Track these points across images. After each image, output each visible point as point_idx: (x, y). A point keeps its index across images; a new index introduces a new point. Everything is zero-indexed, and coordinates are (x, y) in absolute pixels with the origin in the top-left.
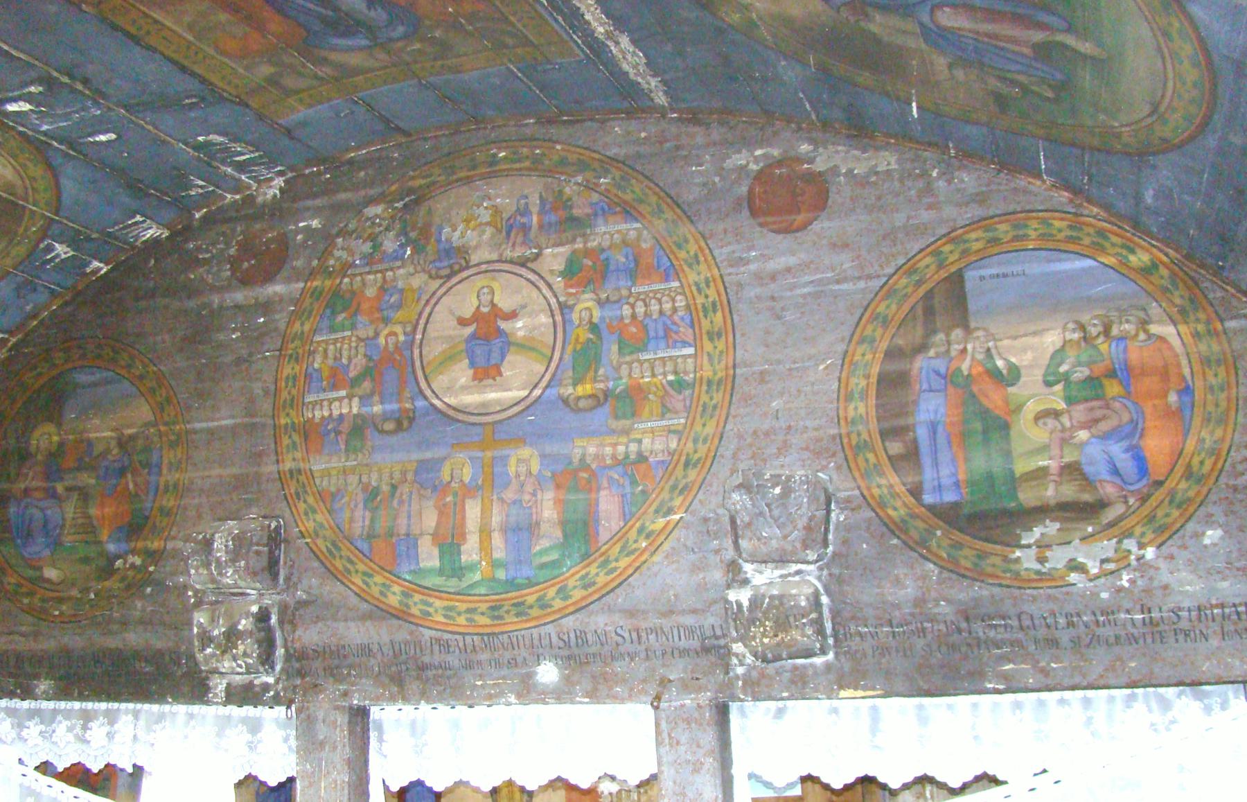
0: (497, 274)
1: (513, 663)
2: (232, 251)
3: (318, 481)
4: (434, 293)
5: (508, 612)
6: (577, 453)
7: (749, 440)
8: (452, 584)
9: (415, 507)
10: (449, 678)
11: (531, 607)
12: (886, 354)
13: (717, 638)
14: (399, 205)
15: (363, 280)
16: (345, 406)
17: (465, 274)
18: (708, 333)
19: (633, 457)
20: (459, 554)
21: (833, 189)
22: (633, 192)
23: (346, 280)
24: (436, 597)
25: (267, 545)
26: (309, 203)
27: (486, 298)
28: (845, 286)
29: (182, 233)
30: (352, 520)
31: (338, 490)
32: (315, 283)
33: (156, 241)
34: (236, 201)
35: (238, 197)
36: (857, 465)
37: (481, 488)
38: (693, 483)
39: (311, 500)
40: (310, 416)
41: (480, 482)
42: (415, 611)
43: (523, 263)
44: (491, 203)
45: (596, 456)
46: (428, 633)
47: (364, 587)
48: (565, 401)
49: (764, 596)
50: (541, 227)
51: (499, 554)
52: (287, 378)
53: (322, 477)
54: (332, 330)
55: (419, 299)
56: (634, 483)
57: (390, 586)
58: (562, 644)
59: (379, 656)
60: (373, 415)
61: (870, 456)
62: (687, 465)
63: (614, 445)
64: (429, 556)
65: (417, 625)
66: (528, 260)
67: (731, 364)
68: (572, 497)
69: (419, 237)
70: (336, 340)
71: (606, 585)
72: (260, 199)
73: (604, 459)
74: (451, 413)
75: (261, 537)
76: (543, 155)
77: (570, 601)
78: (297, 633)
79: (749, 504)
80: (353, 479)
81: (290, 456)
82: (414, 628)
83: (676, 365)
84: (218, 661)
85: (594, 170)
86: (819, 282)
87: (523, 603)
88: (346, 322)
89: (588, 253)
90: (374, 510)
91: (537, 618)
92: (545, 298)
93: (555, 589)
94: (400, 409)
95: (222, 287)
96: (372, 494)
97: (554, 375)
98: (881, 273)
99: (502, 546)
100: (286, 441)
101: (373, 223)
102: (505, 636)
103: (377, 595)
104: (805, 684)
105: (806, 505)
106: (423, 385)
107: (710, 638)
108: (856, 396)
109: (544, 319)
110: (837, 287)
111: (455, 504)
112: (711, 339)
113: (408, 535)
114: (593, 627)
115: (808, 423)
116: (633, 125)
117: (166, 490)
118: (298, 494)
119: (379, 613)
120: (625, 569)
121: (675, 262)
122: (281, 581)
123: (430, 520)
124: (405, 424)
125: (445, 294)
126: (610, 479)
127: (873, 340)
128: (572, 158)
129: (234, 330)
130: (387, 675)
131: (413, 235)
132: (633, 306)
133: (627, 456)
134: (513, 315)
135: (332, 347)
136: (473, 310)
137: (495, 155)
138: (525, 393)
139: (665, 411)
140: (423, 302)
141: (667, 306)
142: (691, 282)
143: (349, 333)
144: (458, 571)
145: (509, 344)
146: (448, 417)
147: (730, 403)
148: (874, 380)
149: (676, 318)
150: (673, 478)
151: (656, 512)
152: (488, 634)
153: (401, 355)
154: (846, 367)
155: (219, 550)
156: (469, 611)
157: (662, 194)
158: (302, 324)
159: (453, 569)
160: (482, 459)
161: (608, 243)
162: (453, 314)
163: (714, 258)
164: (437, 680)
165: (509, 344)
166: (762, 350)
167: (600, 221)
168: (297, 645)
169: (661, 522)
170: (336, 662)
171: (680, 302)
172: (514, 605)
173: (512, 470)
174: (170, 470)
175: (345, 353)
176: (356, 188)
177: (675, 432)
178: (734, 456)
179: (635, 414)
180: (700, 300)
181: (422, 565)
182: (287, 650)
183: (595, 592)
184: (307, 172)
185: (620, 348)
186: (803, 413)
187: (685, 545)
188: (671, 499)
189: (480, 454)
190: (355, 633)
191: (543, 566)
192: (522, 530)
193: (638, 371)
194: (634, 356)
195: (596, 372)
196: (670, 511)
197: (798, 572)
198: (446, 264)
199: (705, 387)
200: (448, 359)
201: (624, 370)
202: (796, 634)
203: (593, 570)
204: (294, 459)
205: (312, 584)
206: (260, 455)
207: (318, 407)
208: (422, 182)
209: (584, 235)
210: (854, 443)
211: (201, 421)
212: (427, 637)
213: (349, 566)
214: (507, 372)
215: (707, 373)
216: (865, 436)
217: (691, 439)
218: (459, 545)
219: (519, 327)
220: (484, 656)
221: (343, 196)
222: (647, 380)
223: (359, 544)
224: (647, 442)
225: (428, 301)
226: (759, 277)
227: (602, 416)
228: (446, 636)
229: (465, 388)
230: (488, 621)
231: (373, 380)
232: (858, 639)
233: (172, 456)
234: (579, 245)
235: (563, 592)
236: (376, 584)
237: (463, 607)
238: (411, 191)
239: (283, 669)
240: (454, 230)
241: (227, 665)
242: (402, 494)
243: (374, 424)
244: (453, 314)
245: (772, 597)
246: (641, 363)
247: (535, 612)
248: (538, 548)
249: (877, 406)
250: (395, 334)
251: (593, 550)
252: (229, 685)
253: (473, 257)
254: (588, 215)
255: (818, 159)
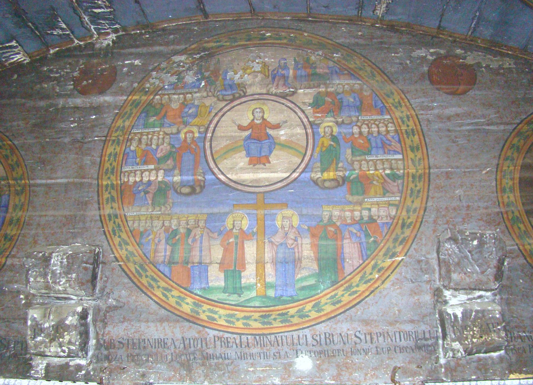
0: (266, 101)
1: (277, 356)
2: (76, 74)
3: (130, 223)
4: (221, 109)
5: (275, 319)
6: (326, 215)
7: (443, 213)
8: (234, 299)
9: (205, 244)
10: (227, 365)
11: (292, 316)
12: (522, 167)
13: (426, 339)
14: (198, 56)
15: (169, 98)
16: (155, 176)
17: (244, 99)
18: (410, 147)
19: (366, 219)
20: (240, 277)
21: (479, 74)
22: (355, 63)
23: (158, 97)
24: (220, 307)
25: (92, 264)
26: (133, 50)
27: (258, 115)
28: (492, 128)
29: (39, 61)
30: (156, 251)
31: (146, 230)
32: (135, 98)
33: (19, 65)
34: (80, 46)
35: (82, 43)
36: (514, 231)
37: (253, 234)
38: (409, 237)
39: (124, 236)
40: (126, 180)
41: (255, 230)
42: (203, 316)
43: (284, 96)
44: (262, 60)
45: (340, 217)
46: (212, 333)
47: (164, 298)
48: (315, 182)
49: (471, 311)
50: (295, 77)
51: (270, 279)
52: (110, 154)
53: (134, 222)
54: (146, 126)
55: (210, 112)
56: (367, 236)
57: (184, 299)
58: (315, 343)
59: (172, 347)
60: (173, 183)
61: (522, 226)
62: (403, 226)
63: (352, 211)
64: (216, 278)
65: (204, 326)
66: (287, 95)
67: (427, 167)
68: (323, 242)
69: (212, 77)
70: (148, 134)
71: (350, 302)
72: (98, 46)
73: (345, 220)
74: (232, 184)
75: (89, 258)
76: (296, 37)
77: (322, 313)
78: (107, 329)
79: (457, 250)
80: (157, 224)
81: (109, 205)
82: (201, 328)
83: (391, 164)
84: (46, 347)
85: (329, 49)
86: (477, 124)
87: (286, 314)
88: (156, 122)
89: (328, 94)
90: (173, 245)
91: (296, 324)
92: (300, 118)
93: (311, 304)
94: (194, 180)
95: (66, 95)
96: (172, 236)
97: (307, 165)
98: (513, 122)
99: (273, 273)
100: (106, 195)
101: (179, 65)
102: (273, 336)
103: (174, 305)
104: (487, 370)
105: (494, 252)
106: (212, 165)
107: (421, 339)
108: (508, 190)
109: (300, 131)
110: (487, 128)
111: (236, 244)
112: (412, 151)
113: (200, 263)
114: (339, 332)
115: (480, 204)
116: (353, 28)
117: (11, 223)
118: (114, 231)
119: (175, 317)
120: (364, 292)
121: (386, 104)
122: (97, 291)
123: (217, 253)
124: (198, 189)
125: (229, 110)
126: (351, 233)
127: (513, 159)
128: (315, 41)
129: (73, 122)
130: (178, 362)
131: (207, 74)
132: (360, 128)
133: (362, 218)
134: (277, 127)
135: (145, 137)
136: (249, 121)
137: (264, 35)
138: (287, 175)
139: (385, 192)
140: (213, 114)
141: (383, 129)
142: (398, 117)
143: (158, 129)
144: (238, 290)
145: (275, 144)
146: (230, 187)
147: (428, 189)
148: (517, 181)
149: (389, 137)
150: (394, 233)
151: (385, 255)
152: (259, 335)
153: (196, 145)
154: (498, 173)
155: (55, 265)
156: (246, 318)
157: (374, 66)
158: (124, 121)
159: (235, 288)
160: (257, 215)
161: (341, 90)
162: (235, 123)
163: (411, 105)
164: (217, 367)
165: (275, 144)
166: (445, 159)
167: (335, 77)
168: (107, 338)
169: (389, 261)
170: (137, 351)
171: (391, 128)
172: (279, 315)
173: (278, 223)
174: (15, 209)
175: (154, 142)
176: (167, 44)
177: (393, 205)
178: (435, 222)
179: (365, 192)
180: (404, 128)
181: (210, 284)
182: (98, 341)
183: (341, 307)
184: (133, 32)
185: (352, 152)
186: (476, 198)
187: (406, 277)
188: (395, 247)
189: (255, 212)
190: (153, 331)
191: (303, 288)
192: (289, 263)
193: (366, 166)
194: (363, 157)
195: (337, 164)
196: (394, 255)
197: (480, 297)
198: (230, 93)
199: (410, 179)
200: (231, 150)
201: (356, 165)
202: (494, 336)
203: (340, 292)
204: (112, 208)
205: (122, 293)
206: (86, 203)
207: (133, 174)
208: (214, 45)
209: (325, 84)
210: (510, 218)
211: (42, 179)
212: (211, 335)
213: (152, 282)
214: (273, 159)
215: (412, 171)
216: (517, 213)
217: (405, 210)
218: (240, 272)
219: (282, 134)
220: (255, 350)
221: (157, 48)
222: (371, 172)
223: (161, 268)
224: (374, 210)
225: (216, 114)
226: (439, 117)
227: (342, 192)
228: (226, 335)
229: (242, 169)
230: (260, 325)
231: (174, 160)
232: (519, 340)
233: (17, 200)
234: (322, 89)
235: (317, 307)
236: (173, 296)
237: (240, 315)
238: (204, 49)
239: (93, 355)
240: (236, 73)
241: (53, 349)
242: (195, 235)
243: (174, 188)
244: (235, 123)
245: (477, 311)
246: (368, 162)
247: (295, 320)
248: (299, 276)
249: (521, 197)
250: (192, 132)
251: (340, 278)
252: (48, 365)
253: (248, 91)
254: (327, 73)
255: (468, 58)
